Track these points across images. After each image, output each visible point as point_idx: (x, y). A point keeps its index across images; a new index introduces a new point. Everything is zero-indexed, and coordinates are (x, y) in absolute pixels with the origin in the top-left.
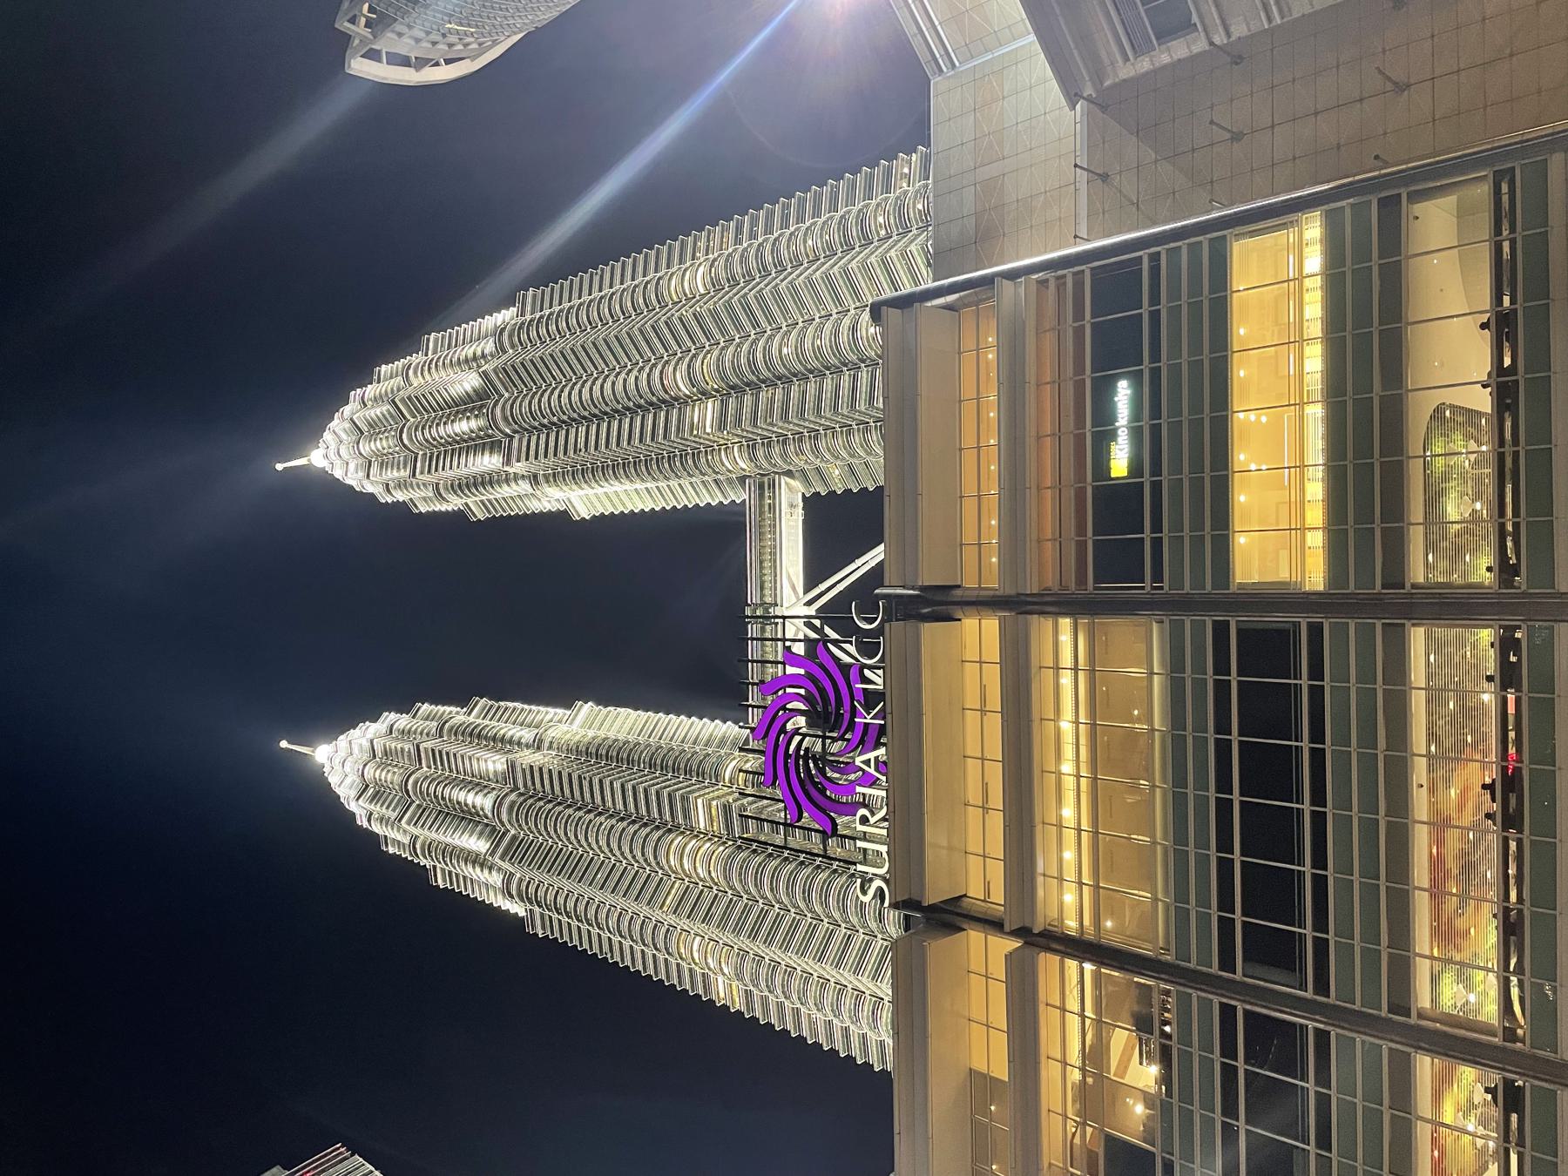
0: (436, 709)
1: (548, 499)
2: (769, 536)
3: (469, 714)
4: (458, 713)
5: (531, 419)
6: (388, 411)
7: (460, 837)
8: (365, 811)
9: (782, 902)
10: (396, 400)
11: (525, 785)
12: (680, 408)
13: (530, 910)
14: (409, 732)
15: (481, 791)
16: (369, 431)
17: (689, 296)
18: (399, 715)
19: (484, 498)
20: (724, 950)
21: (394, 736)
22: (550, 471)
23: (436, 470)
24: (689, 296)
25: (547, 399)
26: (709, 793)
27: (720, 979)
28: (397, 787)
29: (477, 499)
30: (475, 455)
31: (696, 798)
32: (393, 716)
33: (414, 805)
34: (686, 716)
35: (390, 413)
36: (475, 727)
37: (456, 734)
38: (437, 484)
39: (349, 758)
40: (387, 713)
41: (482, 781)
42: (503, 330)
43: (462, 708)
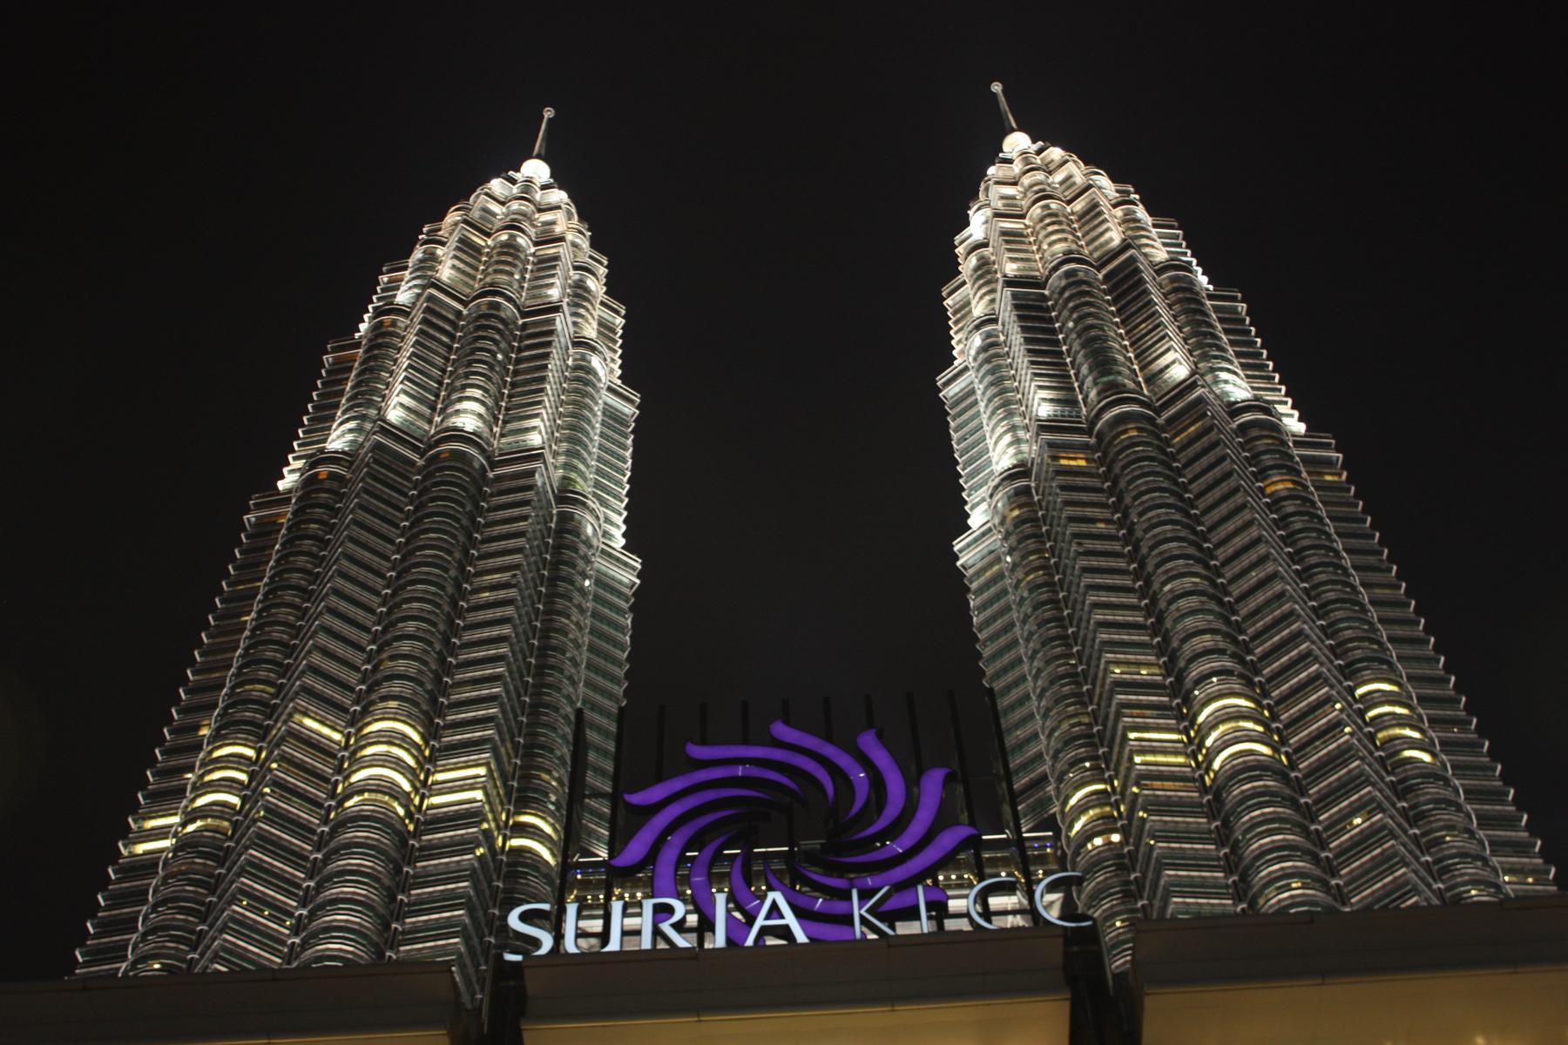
0: (617, 337)
1: (963, 340)
2: (953, 877)
3: (610, 389)
4: (612, 371)
5: (1129, 477)
6: (1111, 240)
7: (402, 405)
8: (447, 235)
9: (318, 893)
10: (1132, 251)
11: (499, 478)
12: (1171, 708)
13: (290, 499)
14: (577, 455)
15: (488, 408)
16: (1073, 213)
17: (1389, 762)
18: (604, 280)
19: (982, 405)
20: (226, 824)
21: (571, 351)
22: (1036, 499)
23: (1009, 250)
24: (1389, 762)
25: (1174, 517)
26: (495, 786)
27: (176, 819)
28: (488, 280)
29: (982, 405)
30: (1051, 400)
31: (487, 765)
32: (602, 271)
33: (460, 307)
34: (627, 505)
35: (1107, 242)
36: (587, 310)
37: (573, 415)
38: (995, 321)
39: (532, 207)
40: (606, 263)
41: (506, 399)
42: (1267, 411)
43: (619, 378)
